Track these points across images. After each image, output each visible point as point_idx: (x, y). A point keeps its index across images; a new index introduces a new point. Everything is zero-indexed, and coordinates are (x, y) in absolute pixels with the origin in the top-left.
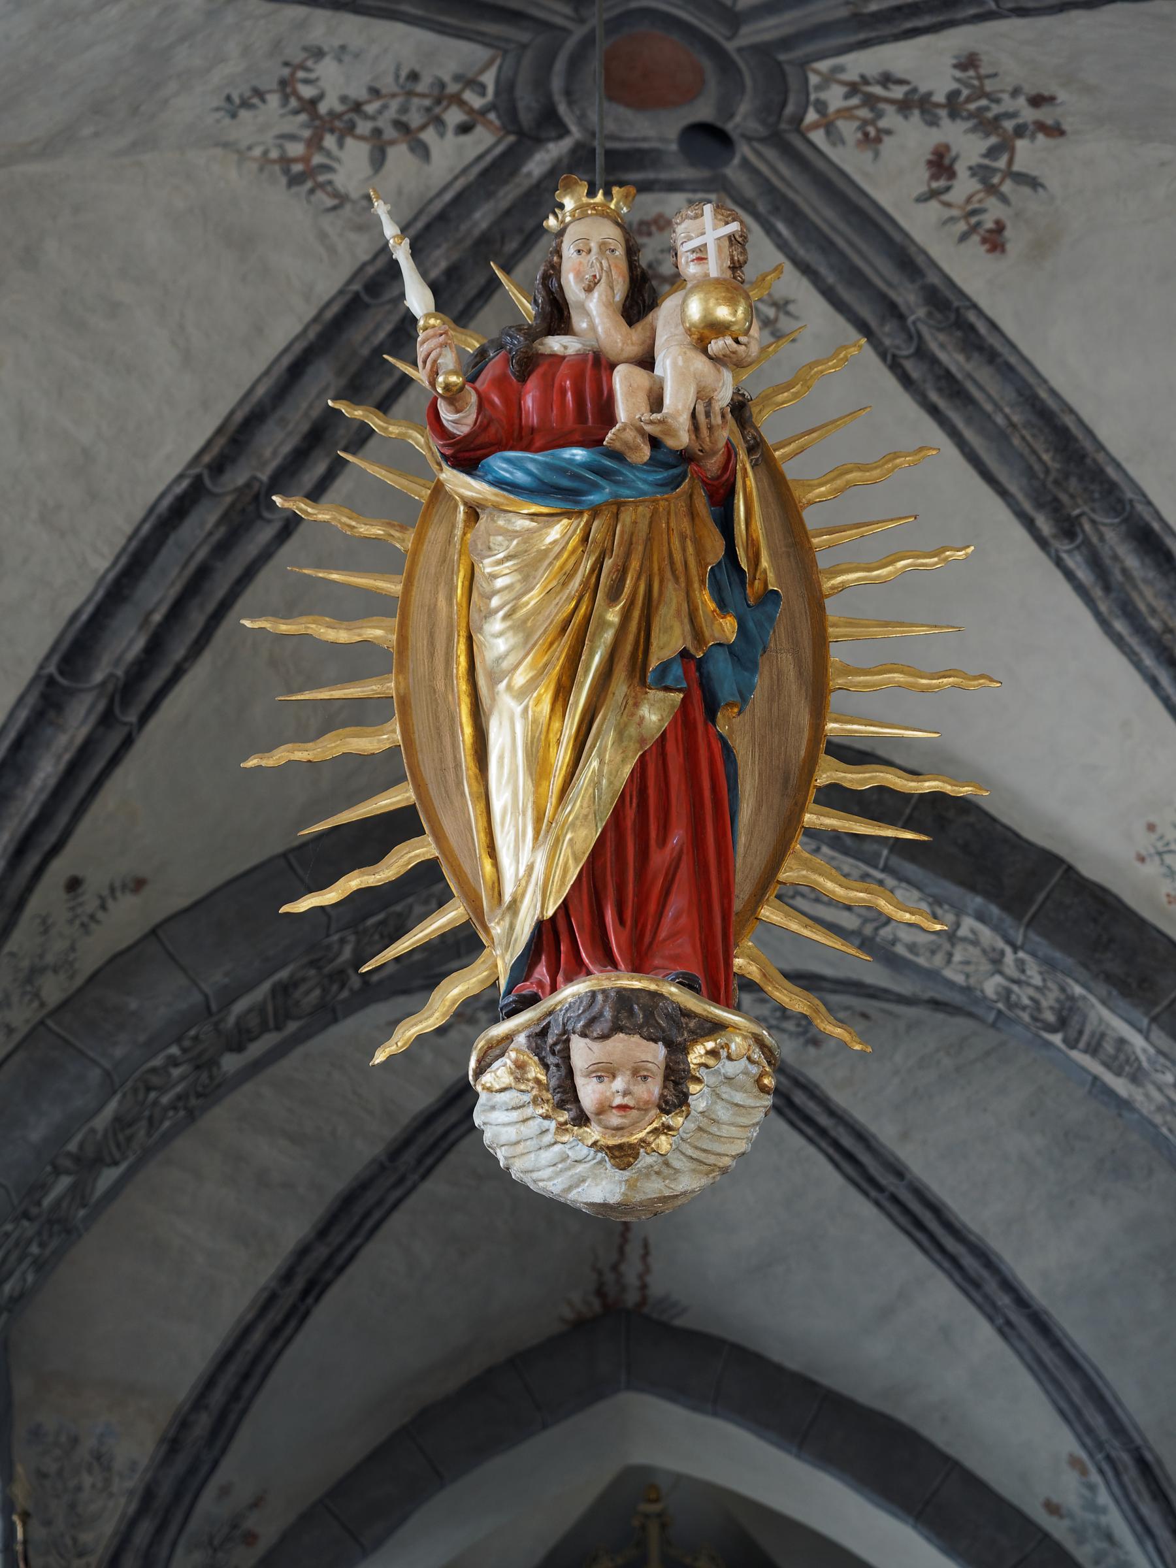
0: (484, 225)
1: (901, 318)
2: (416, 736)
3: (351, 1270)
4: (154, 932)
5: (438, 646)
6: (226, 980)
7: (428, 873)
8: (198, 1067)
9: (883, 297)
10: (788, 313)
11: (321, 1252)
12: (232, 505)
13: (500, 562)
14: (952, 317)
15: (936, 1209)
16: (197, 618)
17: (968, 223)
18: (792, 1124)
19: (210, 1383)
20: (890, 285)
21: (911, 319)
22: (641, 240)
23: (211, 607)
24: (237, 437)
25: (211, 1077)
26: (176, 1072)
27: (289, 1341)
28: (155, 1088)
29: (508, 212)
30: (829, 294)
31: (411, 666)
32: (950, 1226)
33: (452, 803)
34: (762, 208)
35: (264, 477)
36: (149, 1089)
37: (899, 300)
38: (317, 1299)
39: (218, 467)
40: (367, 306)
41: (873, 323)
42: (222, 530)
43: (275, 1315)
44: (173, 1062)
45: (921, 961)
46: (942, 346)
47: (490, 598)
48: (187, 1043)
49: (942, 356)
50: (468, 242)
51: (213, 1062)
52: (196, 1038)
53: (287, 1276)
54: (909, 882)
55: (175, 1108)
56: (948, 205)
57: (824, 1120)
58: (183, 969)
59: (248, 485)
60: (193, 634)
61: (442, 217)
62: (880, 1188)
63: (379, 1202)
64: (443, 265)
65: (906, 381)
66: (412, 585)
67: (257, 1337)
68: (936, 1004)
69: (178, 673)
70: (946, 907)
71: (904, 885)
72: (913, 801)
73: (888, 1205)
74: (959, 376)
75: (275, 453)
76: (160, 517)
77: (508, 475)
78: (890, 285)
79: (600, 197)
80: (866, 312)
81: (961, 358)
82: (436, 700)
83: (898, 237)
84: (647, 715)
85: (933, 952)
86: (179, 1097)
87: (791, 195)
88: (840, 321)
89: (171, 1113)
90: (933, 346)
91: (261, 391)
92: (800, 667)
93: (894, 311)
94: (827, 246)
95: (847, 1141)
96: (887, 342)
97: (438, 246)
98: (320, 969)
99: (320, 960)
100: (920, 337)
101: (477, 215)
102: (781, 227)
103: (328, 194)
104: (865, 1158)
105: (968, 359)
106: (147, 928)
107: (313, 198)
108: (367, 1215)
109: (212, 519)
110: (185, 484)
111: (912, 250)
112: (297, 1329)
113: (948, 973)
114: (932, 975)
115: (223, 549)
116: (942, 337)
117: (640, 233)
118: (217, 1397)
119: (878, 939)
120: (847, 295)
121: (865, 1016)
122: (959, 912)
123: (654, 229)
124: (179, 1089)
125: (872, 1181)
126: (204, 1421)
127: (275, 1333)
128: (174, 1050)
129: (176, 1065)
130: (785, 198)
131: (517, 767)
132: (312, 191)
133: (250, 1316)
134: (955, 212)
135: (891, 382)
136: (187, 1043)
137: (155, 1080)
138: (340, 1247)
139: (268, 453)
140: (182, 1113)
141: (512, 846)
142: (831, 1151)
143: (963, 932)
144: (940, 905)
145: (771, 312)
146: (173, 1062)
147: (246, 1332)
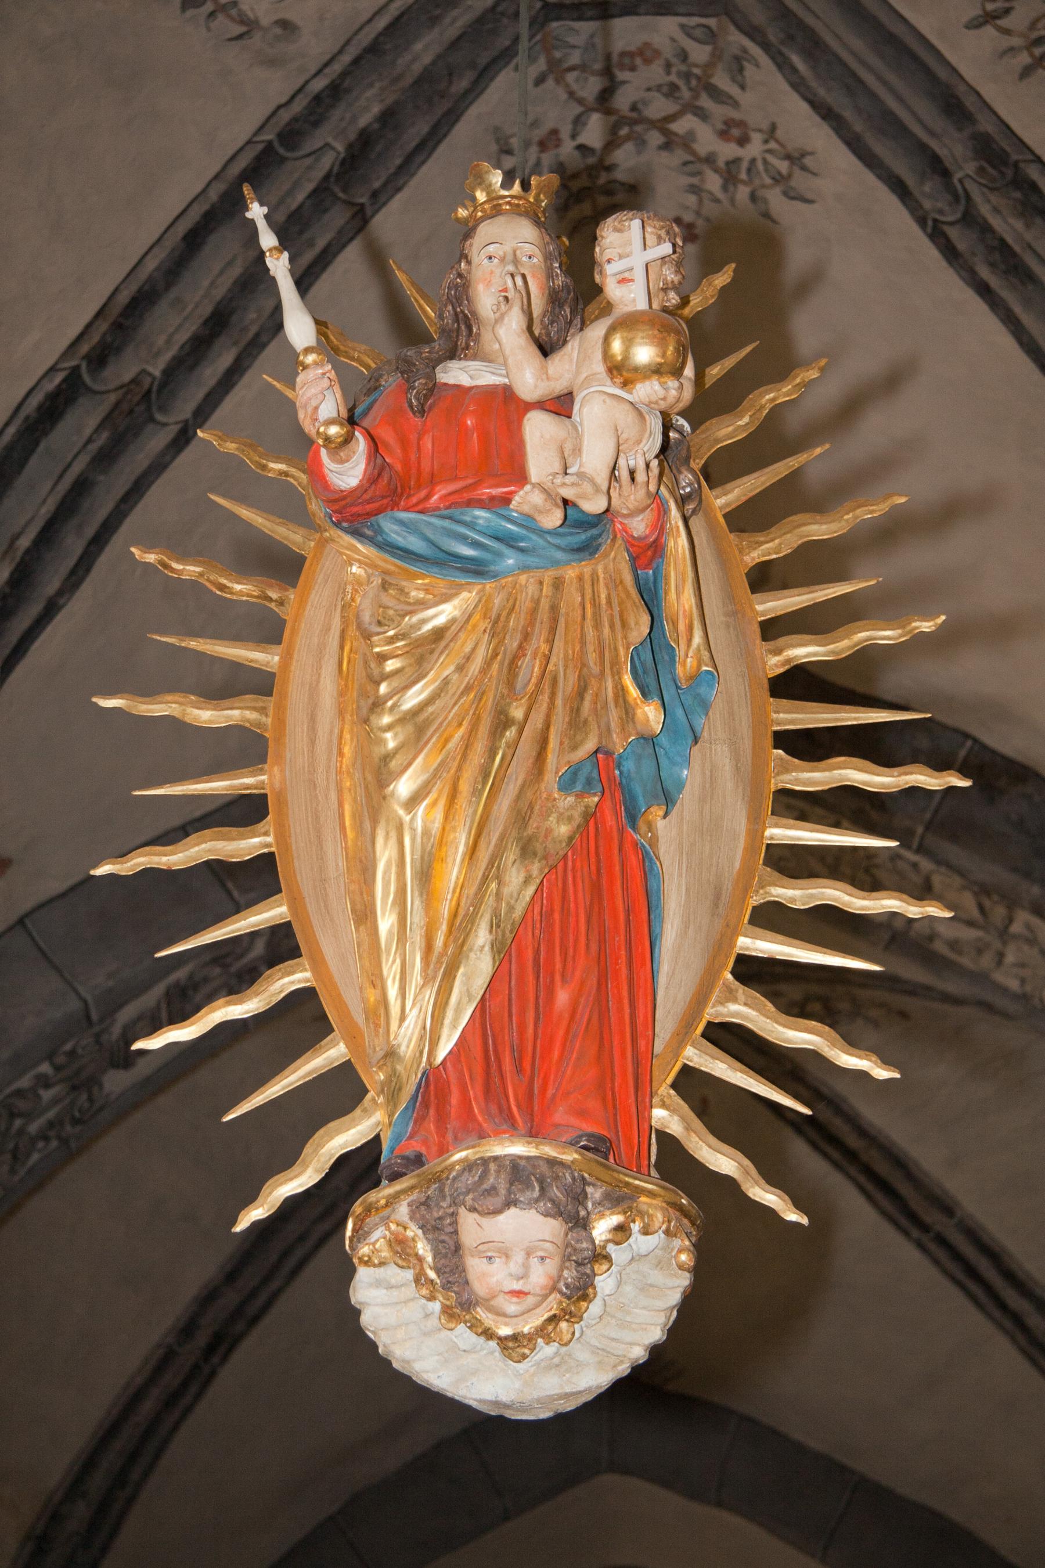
0: (427, 59)
1: (945, 173)
2: (293, 839)
3: (267, 1321)
4: (21, 922)
5: (320, 733)
6: (111, 983)
7: (303, 1000)
8: (74, 1088)
9: (923, 147)
10: (804, 168)
11: (231, 1298)
12: (117, 404)
13: (391, 640)
14: (1010, 173)
15: (993, 1254)
16: (73, 544)
17: (1032, 55)
18: (815, 1146)
19: (89, 1463)
20: (932, 133)
21: (958, 176)
22: (621, 75)
23: (90, 532)
24: (123, 319)
25: (91, 1100)
26: (47, 1095)
27: (188, 1410)
28: (20, 1115)
29: (454, 44)
30: (855, 145)
31: (288, 755)
32: (1010, 1276)
33: (332, 920)
34: (773, 35)
35: (156, 370)
36: (12, 1116)
37: (942, 152)
38: (225, 1358)
39: (99, 359)
40: (283, 160)
41: (910, 180)
42: (105, 435)
43: (171, 1379)
44: (44, 1082)
45: (966, 961)
46: (996, 210)
47: (378, 684)
48: (60, 1059)
49: (995, 222)
50: (409, 80)
51: (93, 1082)
52: (72, 1054)
53: (187, 1330)
54: (949, 866)
55: (46, 1139)
56: (1007, 32)
57: (853, 1141)
58: (58, 970)
59: (135, 381)
60: (71, 562)
61: (374, 49)
62: (924, 1228)
63: (302, 1238)
64: (376, 109)
65: (950, 253)
66: (291, 658)
67: (148, 1406)
68: (988, 1007)
69: (51, 610)
70: (995, 897)
71: (943, 869)
72: (937, 799)
73: (932, 1247)
74: (1017, 248)
75: (169, 342)
76: (27, 418)
77: (400, 539)
78: (932, 133)
79: (517, 187)
80: (902, 168)
81: (1019, 225)
82: (316, 797)
83: (942, 73)
84: (554, 825)
85: (980, 951)
86: (51, 1124)
87: (809, 20)
88: (870, 178)
89: (41, 1144)
90: (984, 210)
91: (151, 265)
92: (737, 761)
93: (938, 168)
94: (853, 85)
95: (883, 1168)
96: (927, 204)
97: (371, 85)
98: (225, 966)
99: (227, 955)
100: (968, 197)
101: (418, 46)
102: (796, 60)
103: (233, 19)
104: (905, 1189)
105: (1028, 226)
106: (13, 918)
107: (213, 25)
108: (285, 1254)
109: (92, 423)
110: (58, 378)
111: (961, 89)
112: (198, 1396)
113: (999, 977)
114: (981, 978)
115: (106, 458)
116: (994, 198)
117: (622, 67)
118: (98, 1482)
119: (912, 933)
120: (880, 147)
121: (903, 1015)
122: (1012, 903)
123: (638, 61)
124: (51, 1114)
125: (913, 1217)
126: (81, 1512)
127: (171, 1400)
128: (45, 1068)
129: (47, 1086)
130: (801, 24)
131: (405, 885)
132: (212, 15)
133: (139, 1380)
134: (1016, 41)
135: (932, 253)
136: (60, 1059)
137: (21, 1105)
138: (253, 1294)
139: (161, 341)
140: (54, 1143)
141: (398, 977)
142: (862, 1179)
143: (1016, 928)
144: (988, 894)
145: (783, 166)
146: (44, 1082)
147: (137, 1397)
